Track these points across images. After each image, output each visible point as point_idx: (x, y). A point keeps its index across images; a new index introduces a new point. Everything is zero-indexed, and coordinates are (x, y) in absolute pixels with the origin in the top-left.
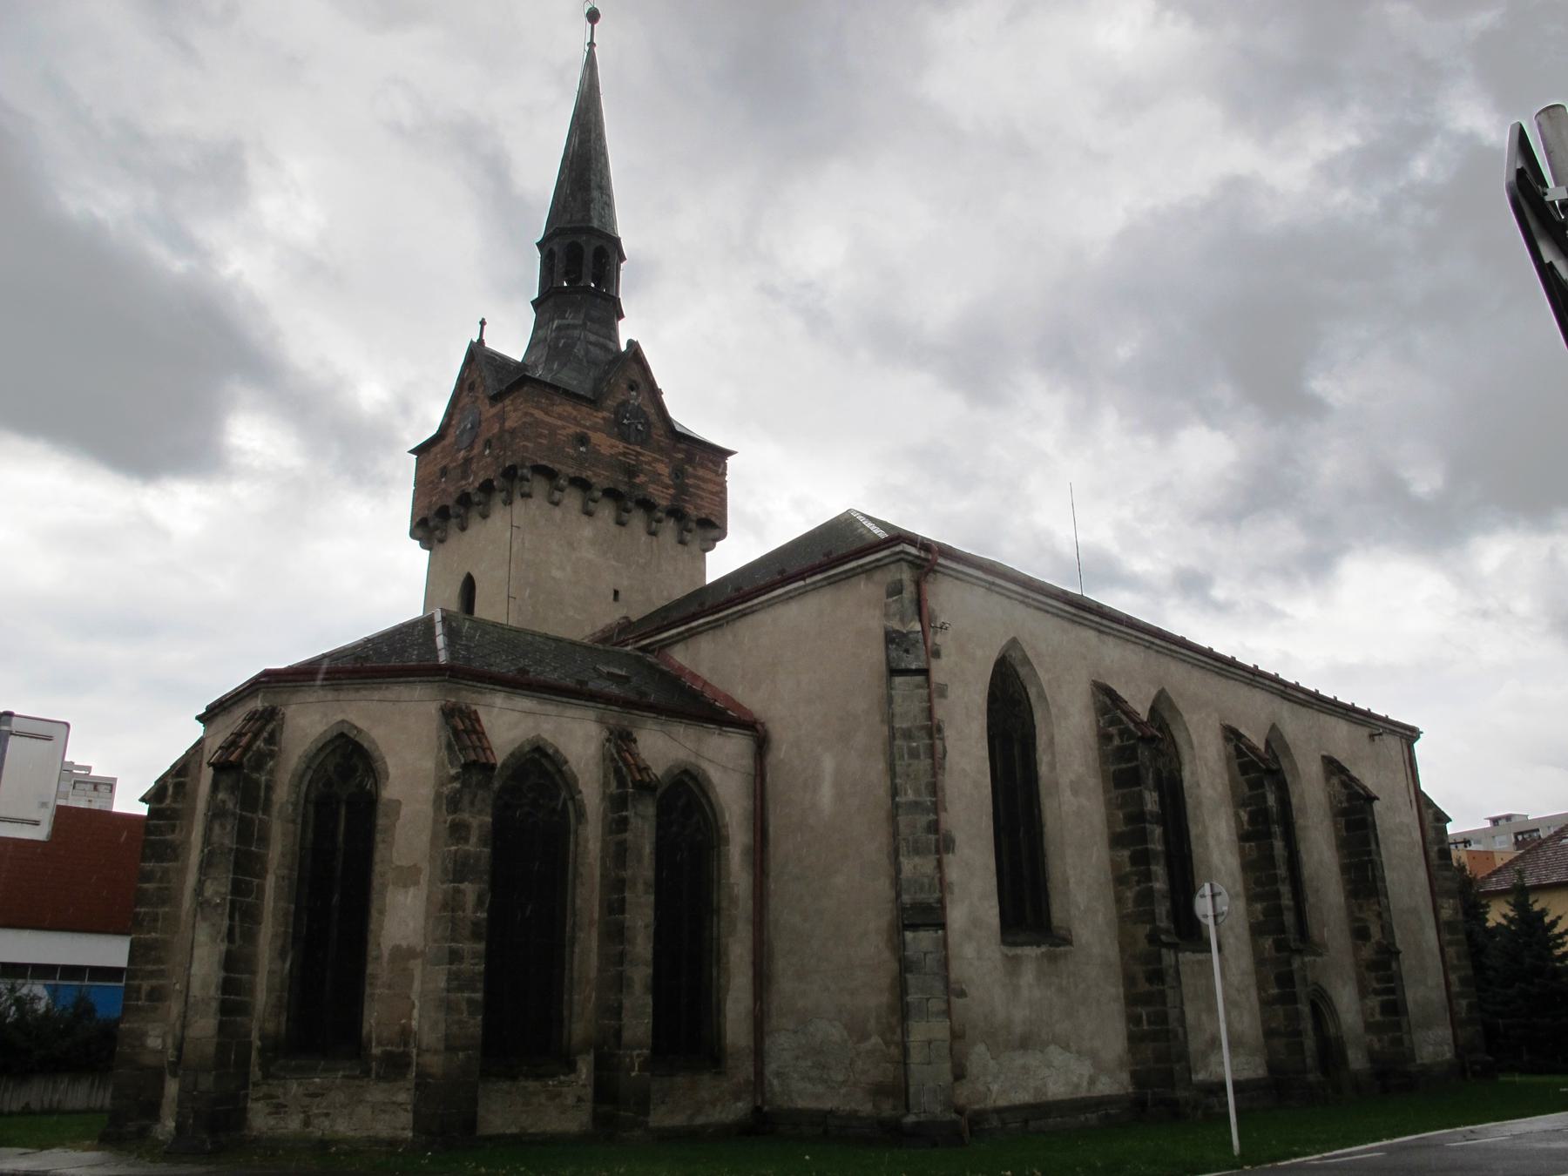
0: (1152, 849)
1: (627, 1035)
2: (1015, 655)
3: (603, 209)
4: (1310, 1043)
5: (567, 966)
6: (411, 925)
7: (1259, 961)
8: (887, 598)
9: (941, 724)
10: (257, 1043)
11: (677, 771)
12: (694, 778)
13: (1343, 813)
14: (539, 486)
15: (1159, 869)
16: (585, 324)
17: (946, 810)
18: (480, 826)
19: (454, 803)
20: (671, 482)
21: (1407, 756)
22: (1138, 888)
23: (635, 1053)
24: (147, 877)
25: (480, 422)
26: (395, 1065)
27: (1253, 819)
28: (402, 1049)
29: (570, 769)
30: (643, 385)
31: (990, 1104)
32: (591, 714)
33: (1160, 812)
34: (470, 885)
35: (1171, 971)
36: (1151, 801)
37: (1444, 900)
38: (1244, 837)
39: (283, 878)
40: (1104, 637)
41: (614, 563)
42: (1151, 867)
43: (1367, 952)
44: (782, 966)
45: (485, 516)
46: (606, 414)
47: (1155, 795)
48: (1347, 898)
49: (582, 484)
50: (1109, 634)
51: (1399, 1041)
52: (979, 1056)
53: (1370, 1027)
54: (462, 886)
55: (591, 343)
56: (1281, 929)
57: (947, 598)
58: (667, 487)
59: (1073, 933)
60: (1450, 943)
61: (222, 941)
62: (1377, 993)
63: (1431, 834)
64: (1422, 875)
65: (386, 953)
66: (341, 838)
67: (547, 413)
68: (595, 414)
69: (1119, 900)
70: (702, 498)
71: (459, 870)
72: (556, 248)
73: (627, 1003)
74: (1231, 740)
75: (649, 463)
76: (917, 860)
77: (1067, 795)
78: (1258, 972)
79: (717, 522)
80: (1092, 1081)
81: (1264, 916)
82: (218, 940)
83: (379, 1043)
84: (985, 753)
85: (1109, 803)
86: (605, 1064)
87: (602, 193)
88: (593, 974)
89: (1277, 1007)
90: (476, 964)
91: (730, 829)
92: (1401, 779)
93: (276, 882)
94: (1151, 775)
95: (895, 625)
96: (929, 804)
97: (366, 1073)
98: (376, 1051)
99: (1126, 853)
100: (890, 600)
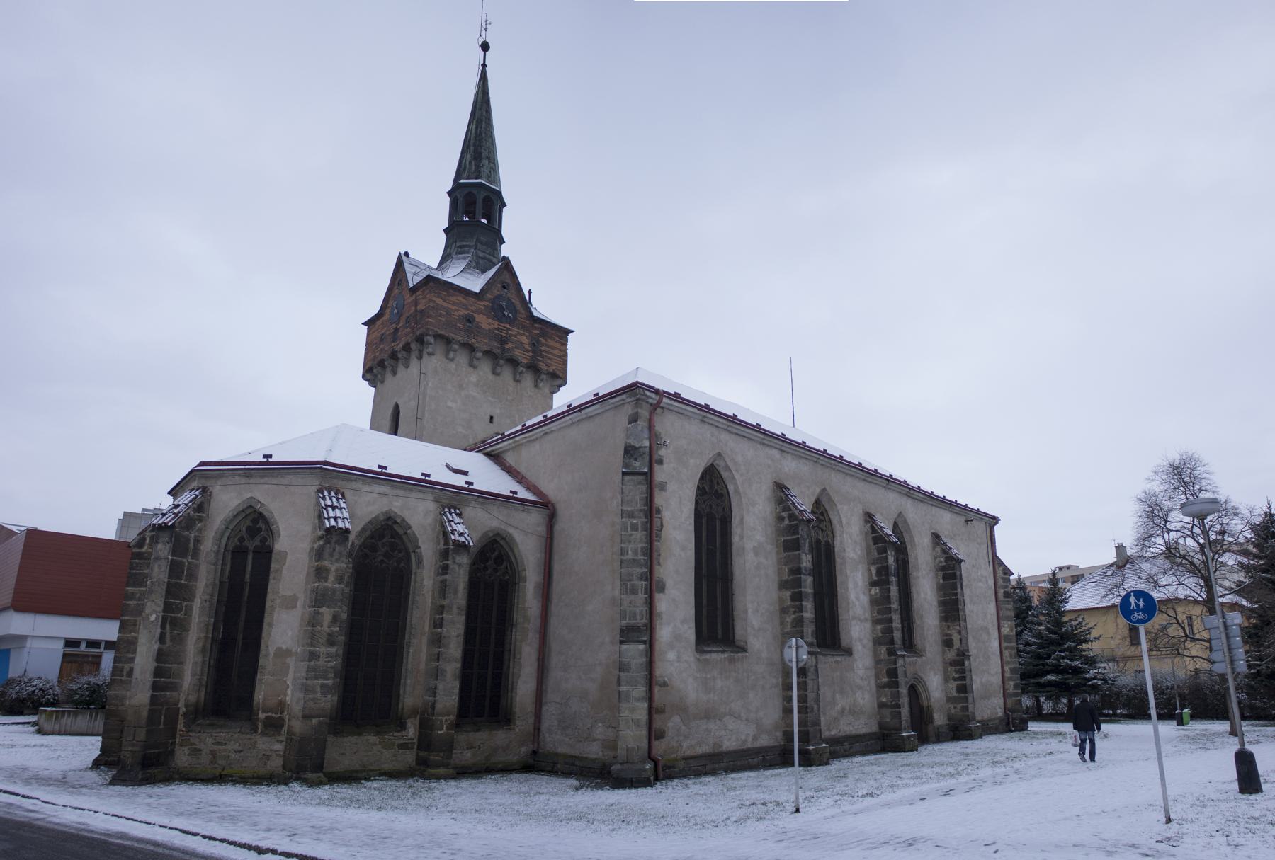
0: (804, 592)
1: (439, 706)
2: (720, 465)
3: (490, 172)
4: (905, 711)
5: (405, 661)
6: (290, 633)
7: (878, 661)
8: (629, 424)
9: (660, 508)
10: (183, 710)
11: (491, 534)
12: (503, 539)
13: (943, 569)
14: (439, 348)
15: (809, 605)
16: (476, 245)
17: (659, 564)
18: (337, 570)
19: (319, 554)
20: (530, 349)
21: (989, 534)
22: (794, 616)
23: (444, 718)
24: (131, 597)
25: (404, 305)
26: (274, 725)
27: (879, 572)
28: (279, 715)
29: (414, 532)
30: (512, 285)
31: (680, 754)
32: (430, 496)
33: (812, 567)
34: (327, 609)
35: (812, 669)
36: (806, 561)
37: (1005, 622)
38: (873, 584)
39: (206, 601)
40: (785, 454)
41: (490, 398)
42: (803, 603)
43: (951, 655)
44: (555, 661)
45: (407, 367)
46: (486, 303)
47: (809, 557)
48: (941, 621)
49: (471, 349)
50: (788, 453)
51: (966, 708)
52: (673, 723)
53: (950, 700)
54: (321, 610)
55: (480, 257)
56: (892, 642)
57: (668, 425)
58: (527, 351)
59: (748, 643)
60: (1006, 648)
61: (156, 643)
62: (955, 679)
63: (1000, 582)
64: (992, 608)
65: (272, 651)
66: (248, 576)
67: (445, 301)
68: (478, 302)
69: (782, 623)
70: (550, 359)
71: (320, 599)
72: (458, 196)
73: (440, 686)
74: (869, 522)
75: (515, 336)
76: (632, 597)
77: (750, 556)
78: (876, 668)
79: (561, 375)
80: (755, 738)
81: (882, 633)
82: (153, 642)
83: (264, 711)
84: (692, 528)
85: (779, 561)
86: (426, 726)
87: (489, 162)
88: (422, 666)
89: (887, 689)
90: (328, 662)
91: (527, 572)
92: (984, 549)
93: (201, 603)
94: (807, 545)
95: (632, 442)
96: (642, 561)
97: (255, 730)
98: (262, 716)
99: (788, 593)
100: (630, 426)
